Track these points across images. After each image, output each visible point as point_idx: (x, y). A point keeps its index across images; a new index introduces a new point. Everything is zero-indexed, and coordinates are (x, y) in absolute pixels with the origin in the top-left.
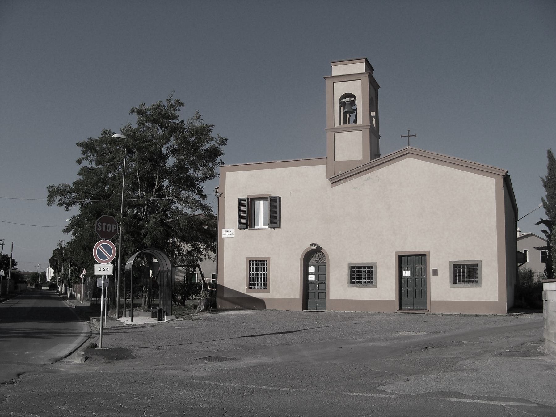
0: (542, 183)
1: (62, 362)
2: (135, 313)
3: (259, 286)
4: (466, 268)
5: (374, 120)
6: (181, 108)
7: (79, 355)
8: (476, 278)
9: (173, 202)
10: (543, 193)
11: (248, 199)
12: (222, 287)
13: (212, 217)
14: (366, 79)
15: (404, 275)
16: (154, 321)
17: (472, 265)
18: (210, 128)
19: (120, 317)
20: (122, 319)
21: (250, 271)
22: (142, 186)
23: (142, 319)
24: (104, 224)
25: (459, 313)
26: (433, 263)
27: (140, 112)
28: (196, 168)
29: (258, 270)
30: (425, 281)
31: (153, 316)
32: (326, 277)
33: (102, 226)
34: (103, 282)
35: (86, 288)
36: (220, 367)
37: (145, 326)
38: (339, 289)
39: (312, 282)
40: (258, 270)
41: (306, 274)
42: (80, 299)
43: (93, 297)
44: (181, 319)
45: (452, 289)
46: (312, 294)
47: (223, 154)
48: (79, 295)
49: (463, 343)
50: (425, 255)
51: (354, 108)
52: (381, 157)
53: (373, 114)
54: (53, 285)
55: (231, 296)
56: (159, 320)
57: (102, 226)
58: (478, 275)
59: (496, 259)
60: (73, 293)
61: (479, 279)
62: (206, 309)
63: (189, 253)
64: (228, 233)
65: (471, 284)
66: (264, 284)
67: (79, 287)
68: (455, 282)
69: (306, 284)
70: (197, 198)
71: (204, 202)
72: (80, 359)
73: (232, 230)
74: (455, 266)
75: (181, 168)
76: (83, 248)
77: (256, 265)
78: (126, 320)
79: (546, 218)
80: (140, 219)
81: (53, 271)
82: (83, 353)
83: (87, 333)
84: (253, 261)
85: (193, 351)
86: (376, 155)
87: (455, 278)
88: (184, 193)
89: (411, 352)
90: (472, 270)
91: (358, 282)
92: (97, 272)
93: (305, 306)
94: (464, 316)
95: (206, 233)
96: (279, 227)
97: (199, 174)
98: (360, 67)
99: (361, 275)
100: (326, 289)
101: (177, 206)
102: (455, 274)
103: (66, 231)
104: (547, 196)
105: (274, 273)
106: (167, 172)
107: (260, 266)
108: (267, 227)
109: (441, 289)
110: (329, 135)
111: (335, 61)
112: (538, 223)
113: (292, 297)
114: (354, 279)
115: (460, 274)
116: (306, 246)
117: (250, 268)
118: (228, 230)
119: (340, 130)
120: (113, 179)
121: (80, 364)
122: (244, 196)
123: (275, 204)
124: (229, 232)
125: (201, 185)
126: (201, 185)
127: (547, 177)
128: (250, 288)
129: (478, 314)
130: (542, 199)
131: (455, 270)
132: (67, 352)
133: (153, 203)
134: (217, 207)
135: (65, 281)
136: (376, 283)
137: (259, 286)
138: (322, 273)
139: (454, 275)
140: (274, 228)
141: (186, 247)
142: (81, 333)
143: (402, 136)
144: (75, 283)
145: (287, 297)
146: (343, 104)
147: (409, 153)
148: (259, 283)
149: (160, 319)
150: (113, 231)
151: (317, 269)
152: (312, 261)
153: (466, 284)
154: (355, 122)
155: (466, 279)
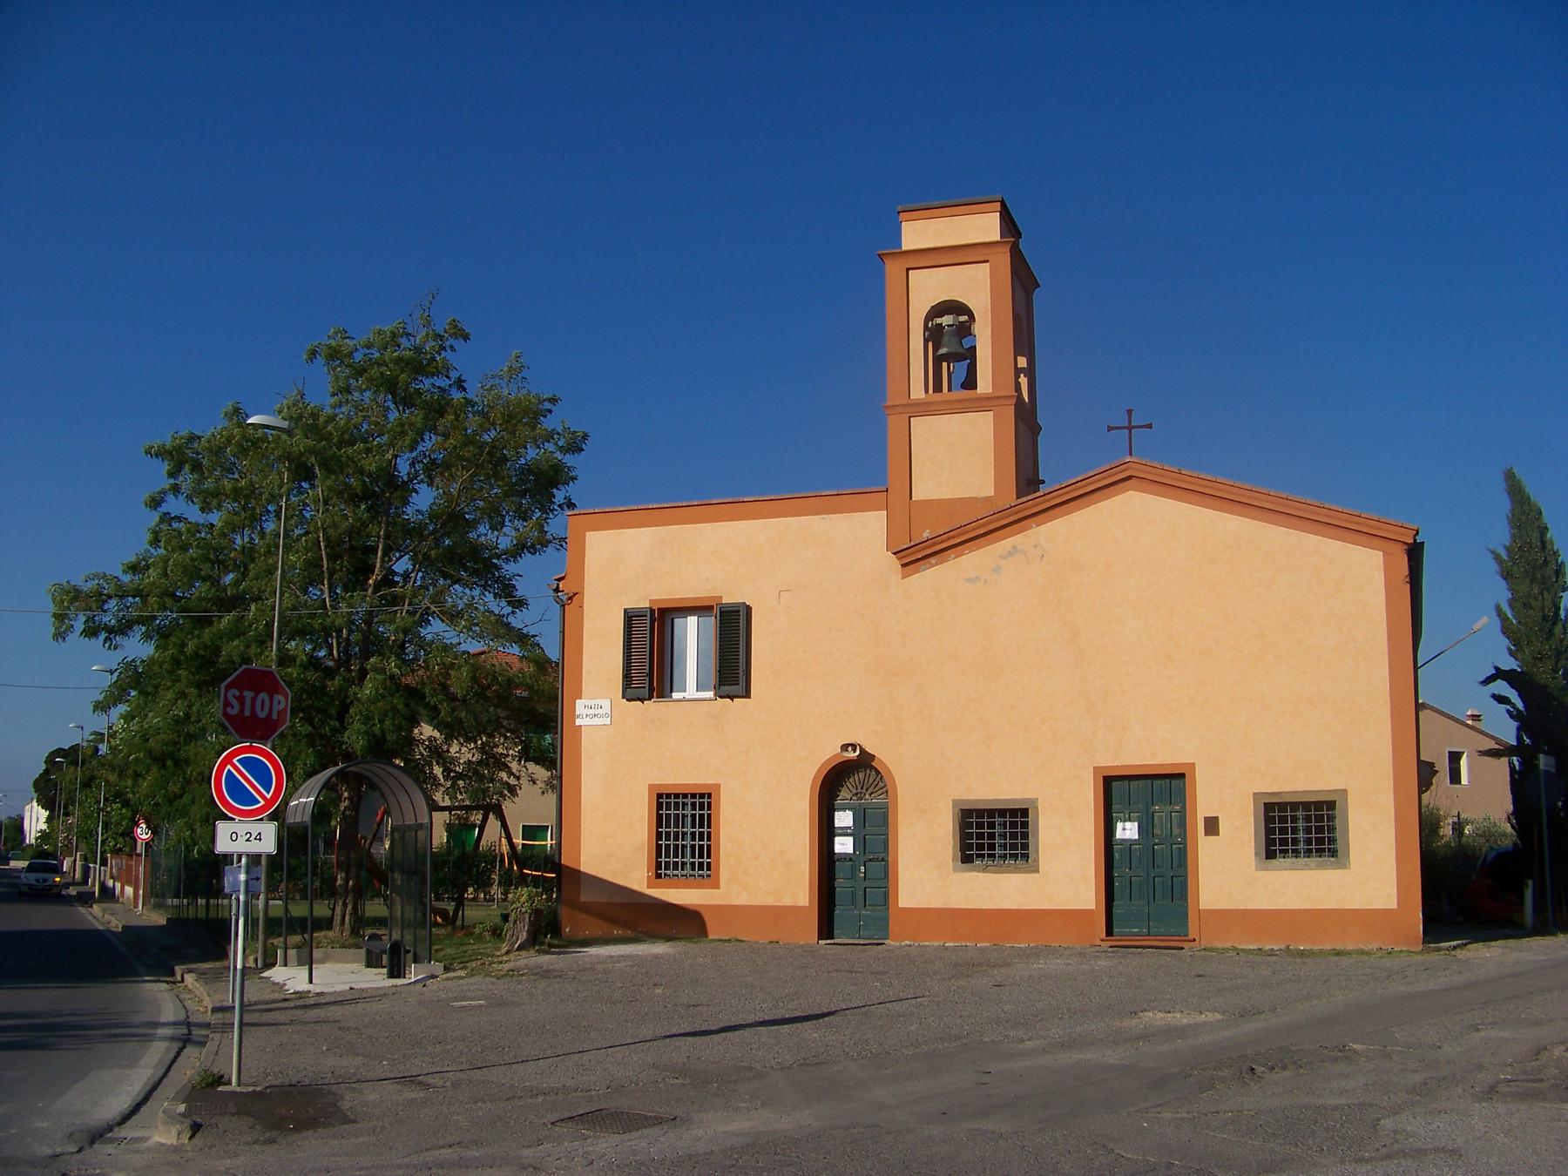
0: (1496, 567)
1: (112, 1140)
2: (317, 953)
3: (688, 870)
4: (1300, 814)
5: (1023, 380)
6: (459, 344)
7: (171, 1117)
8: (1332, 841)
9: (424, 621)
10: (1501, 593)
11: (652, 611)
12: (576, 874)
13: (545, 666)
14: (1004, 258)
15: (1119, 834)
16: (376, 979)
17: (1319, 805)
18: (547, 405)
19: (269, 965)
20: (277, 974)
21: (659, 825)
22: (332, 573)
23: (341, 974)
24: (248, 694)
25: (1283, 946)
26: (1205, 799)
27: (334, 354)
28: (497, 526)
29: (684, 824)
30: (1183, 853)
31: (370, 964)
32: (886, 842)
33: (241, 700)
34: (243, 877)
35: (154, 868)
36: (635, 1153)
37: (354, 998)
38: (927, 874)
39: (845, 857)
40: (684, 824)
41: (826, 831)
42: (131, 904)
43: (177, 896)
44: (462, 973)
45: (1265, 876)
46: (847, 889)
47: (574, 479)
48: (129, 890)
49: (1356, 1052)
50: (1182, 776)
51: (966, 343)
52: (1043, 489)
53: (1022, 362)
54: (45, 857)
55: (604, 899)
56: (392, 975)
57: (241, 700)
58: (1338, 834)
59: (1388, 784)
60: (110, 883)
61: (1339, 845)
62: (533, 941)
63: (473, 770)
64: (593, 711)
65: (1313, 861)
66: (701, 864)
67: (129, 867)
68: (1270, 855)
69: (827, 861)
70: (499, 607)
71: (516, 622)
72: (174, 1132)
73: (606, 703)
74: (1269, 807)
75: (451, 519)
76: (155, 760)
77: (677, 808)
78: (290, 977)
79: (1509, 664)
80: (330, 673)
81: (44, 814)
82: (182, 1108)
83: (175, 1024)
84: (668, 796)
85: (535, 1092)
86: (1033, 486)
87: (1269, 842)
88: (459, 595)
89: (1211, 1087)
90: (1319, 818)
91: (982, 856)
92: (223, 845)
93: (826, 929)
94: (1302, 954)
95: (529, 714)
96: (747, 695)
97: (505, 541)
98: (985, 226)
99: (992, 836)
100: (886, 877)
101: (436, 628)
102: (1269, 831)
103: (101, 707)
104: (1511, 603)
105: (733, 831)
106: (402, 535)
107: (688, 812)
108: (710, 694)
109: (1230, 874)
110: (894, 422)
111: (911, 206)
112: (1488, 680)
113: (787, 902)
114: (970, 847)
115: (1283, 831)
116: (828, 751)
117: (659, 817)
118: (592, 702)
119: (924, 409)
120: (249, 552)
121: (176, 1149)
122: (640, 601)
123: (732, 628)
124: (594, 705)
125: (509, 568)
126: (509, 568)
127: (1508, 549)
128: (658, 876)
129: (1339, 947)
130: (1498, 609)
131: (1268, 820)
132: (121, 1102)
133: (369, 623)
134: (558, 636)
135: (83, 846)
136: (1036, 860)
137: (688, 870)
138: (876, 833)
139: (1267, 834)
140: (732, 698)
141: (463, 753)
142: (156, 1025)
143: (1110, 429)
144: (117, 852)
145: (770, 901)
146: (934, 335)
147: (1130, 477)
148: (688, 859)
149: (396, 971)
150: (275, 716)
151: (861, 817)
152: (844, 794)
153: (1302, 861)
154: (970, 383)
155: (1302, 846)
